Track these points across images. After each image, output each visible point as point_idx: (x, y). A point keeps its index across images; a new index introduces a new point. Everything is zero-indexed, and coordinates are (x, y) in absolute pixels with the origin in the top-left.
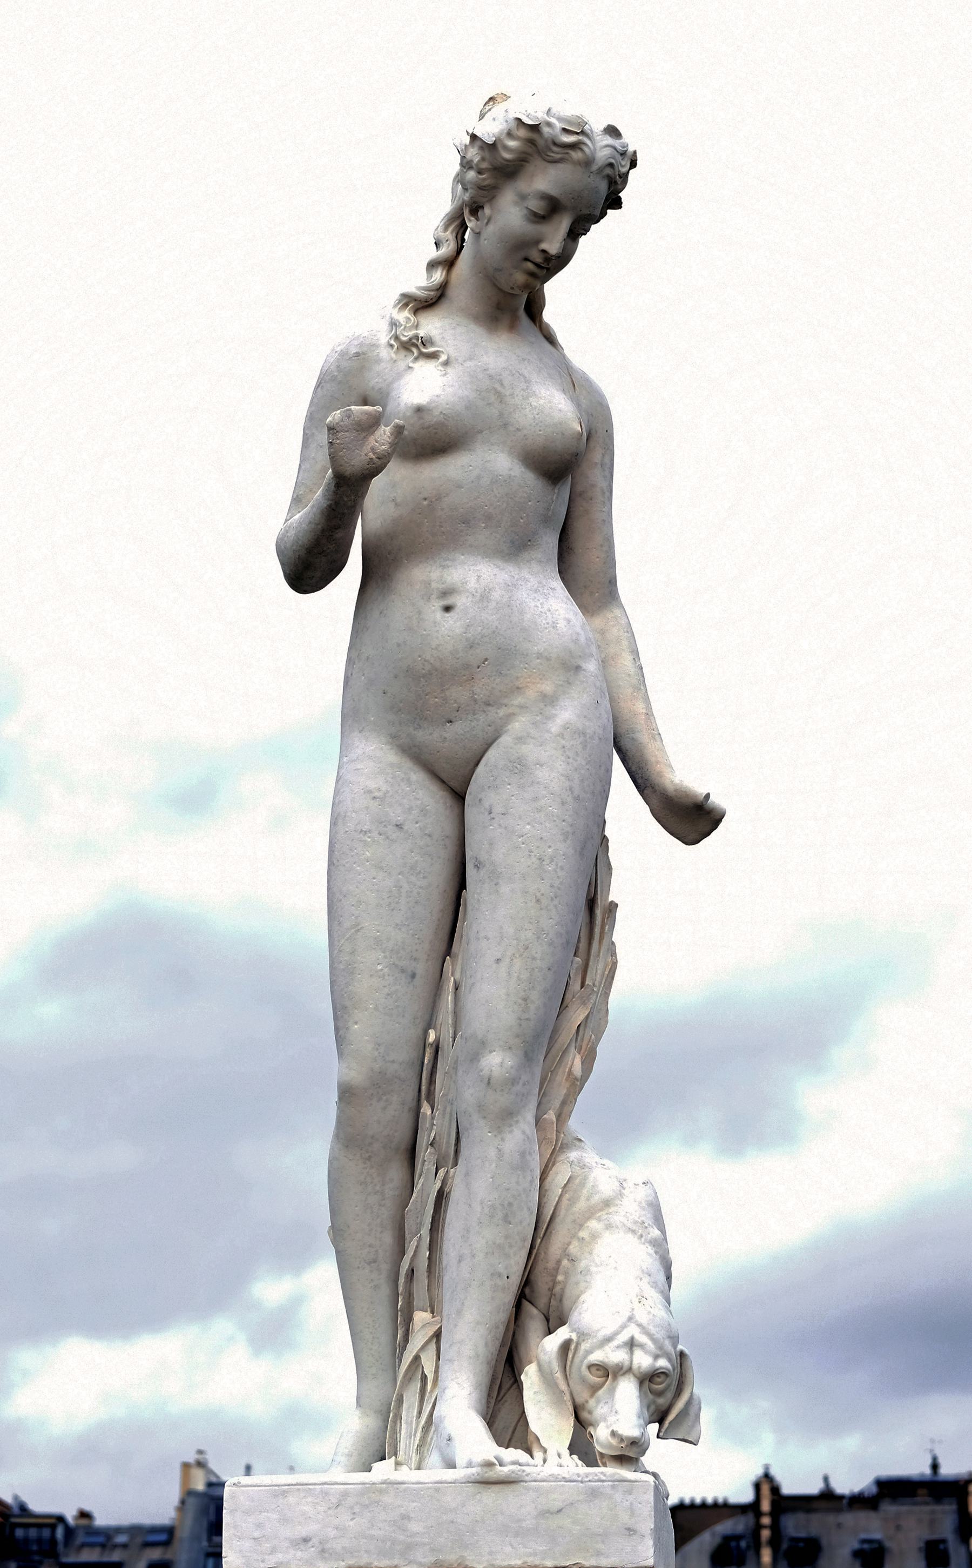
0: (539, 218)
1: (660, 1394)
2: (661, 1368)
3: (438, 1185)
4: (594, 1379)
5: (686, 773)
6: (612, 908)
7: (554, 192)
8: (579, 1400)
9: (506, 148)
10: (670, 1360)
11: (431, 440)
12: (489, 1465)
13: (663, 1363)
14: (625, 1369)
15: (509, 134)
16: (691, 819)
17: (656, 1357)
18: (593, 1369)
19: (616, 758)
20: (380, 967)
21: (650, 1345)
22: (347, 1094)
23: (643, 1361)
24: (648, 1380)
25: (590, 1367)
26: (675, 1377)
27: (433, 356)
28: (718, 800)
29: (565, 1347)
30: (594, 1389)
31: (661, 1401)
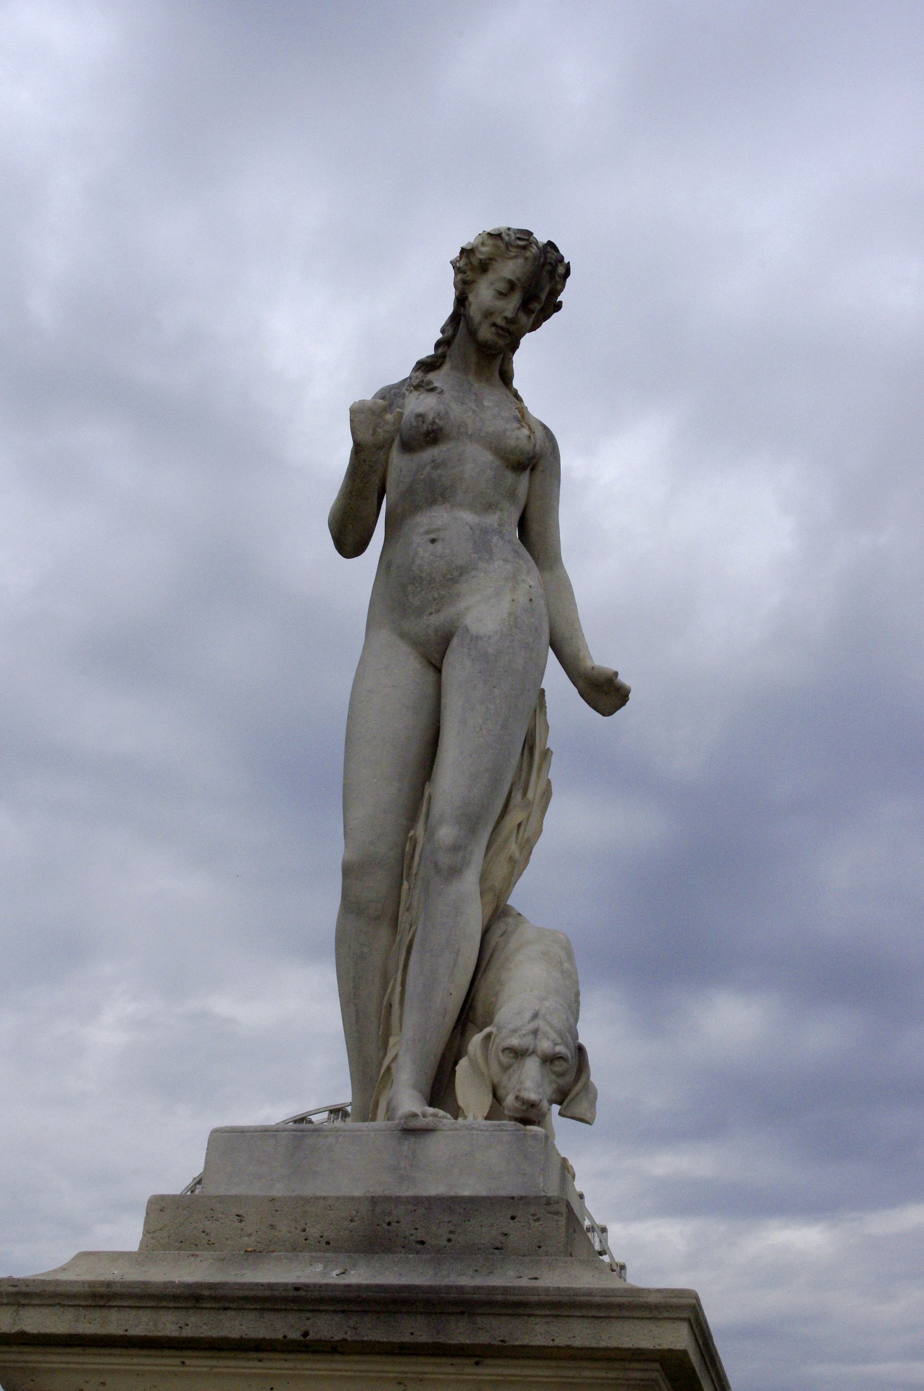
0: (501, 295)
1: (561, 1075)
2: (560, 1053)
3: (409, 938)
4: (505, 1060)
5: (601, 655)
6: (547, 753)
7: (513, 278)
8: (496, 1080)
9: (481, 253)
10: (567, 1046)
11: (430, 435)
12: (415, 1115)
13: (560, 1049)
14: (530, 1051)
15: (483, 244)
16: (605, 693)
17: (556, 1044)
18: (507, 1052)
19: (551, 652)
20: (375, 780)
21: (553, 1035)
22: (348, 871)
23: (545, 1045)
24: (549, 1060)
25: (504, 1050)
26: (573, 1061)
27: (433, 390)
28: (624, 679)
29: (488, 1037)
30: (506, 1068)
31: (562, 1081)
